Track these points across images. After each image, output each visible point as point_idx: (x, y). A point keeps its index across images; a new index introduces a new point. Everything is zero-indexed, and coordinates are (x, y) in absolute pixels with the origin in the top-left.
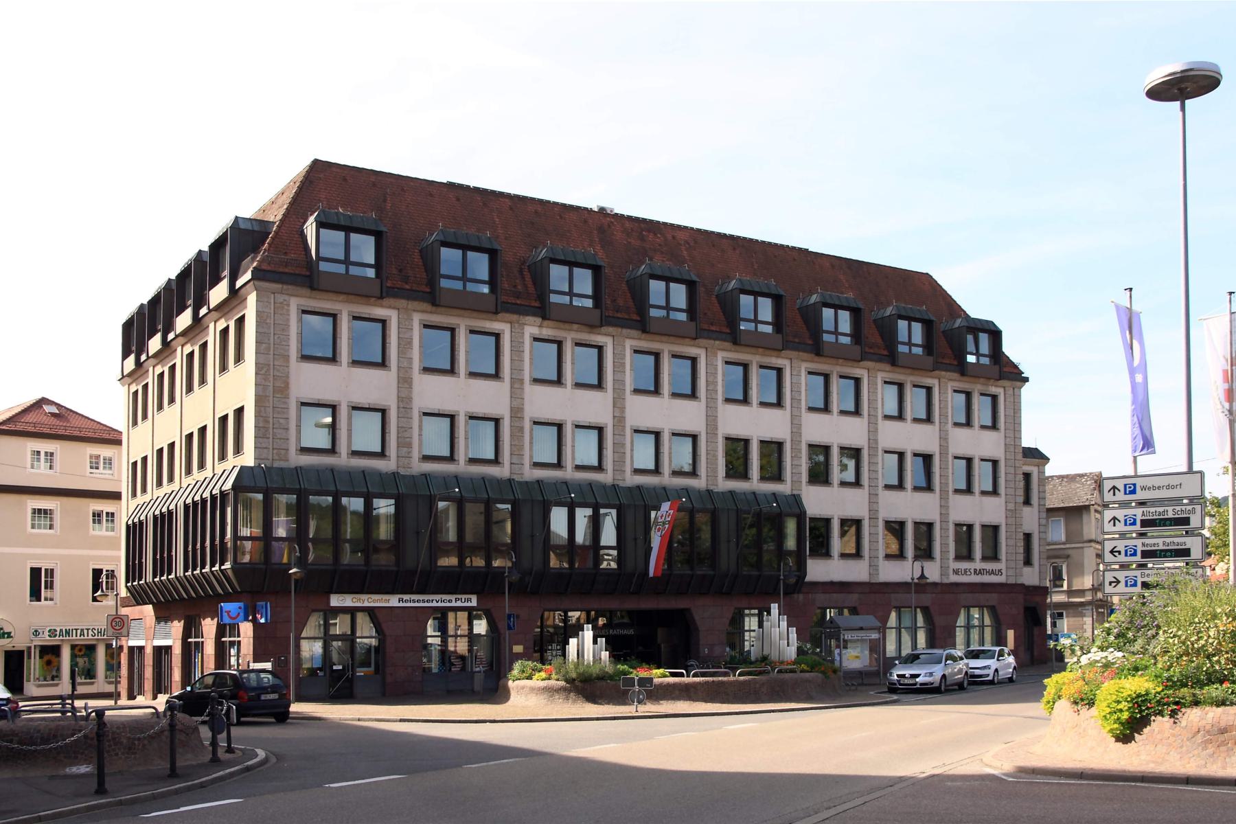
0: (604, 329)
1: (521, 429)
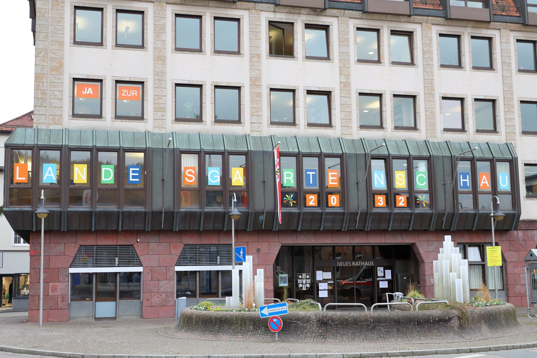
0: (329, 11)
1: (259, 95)
